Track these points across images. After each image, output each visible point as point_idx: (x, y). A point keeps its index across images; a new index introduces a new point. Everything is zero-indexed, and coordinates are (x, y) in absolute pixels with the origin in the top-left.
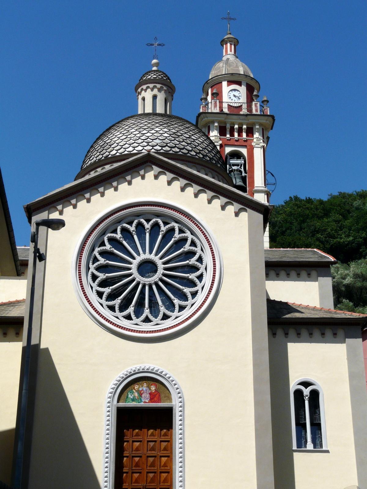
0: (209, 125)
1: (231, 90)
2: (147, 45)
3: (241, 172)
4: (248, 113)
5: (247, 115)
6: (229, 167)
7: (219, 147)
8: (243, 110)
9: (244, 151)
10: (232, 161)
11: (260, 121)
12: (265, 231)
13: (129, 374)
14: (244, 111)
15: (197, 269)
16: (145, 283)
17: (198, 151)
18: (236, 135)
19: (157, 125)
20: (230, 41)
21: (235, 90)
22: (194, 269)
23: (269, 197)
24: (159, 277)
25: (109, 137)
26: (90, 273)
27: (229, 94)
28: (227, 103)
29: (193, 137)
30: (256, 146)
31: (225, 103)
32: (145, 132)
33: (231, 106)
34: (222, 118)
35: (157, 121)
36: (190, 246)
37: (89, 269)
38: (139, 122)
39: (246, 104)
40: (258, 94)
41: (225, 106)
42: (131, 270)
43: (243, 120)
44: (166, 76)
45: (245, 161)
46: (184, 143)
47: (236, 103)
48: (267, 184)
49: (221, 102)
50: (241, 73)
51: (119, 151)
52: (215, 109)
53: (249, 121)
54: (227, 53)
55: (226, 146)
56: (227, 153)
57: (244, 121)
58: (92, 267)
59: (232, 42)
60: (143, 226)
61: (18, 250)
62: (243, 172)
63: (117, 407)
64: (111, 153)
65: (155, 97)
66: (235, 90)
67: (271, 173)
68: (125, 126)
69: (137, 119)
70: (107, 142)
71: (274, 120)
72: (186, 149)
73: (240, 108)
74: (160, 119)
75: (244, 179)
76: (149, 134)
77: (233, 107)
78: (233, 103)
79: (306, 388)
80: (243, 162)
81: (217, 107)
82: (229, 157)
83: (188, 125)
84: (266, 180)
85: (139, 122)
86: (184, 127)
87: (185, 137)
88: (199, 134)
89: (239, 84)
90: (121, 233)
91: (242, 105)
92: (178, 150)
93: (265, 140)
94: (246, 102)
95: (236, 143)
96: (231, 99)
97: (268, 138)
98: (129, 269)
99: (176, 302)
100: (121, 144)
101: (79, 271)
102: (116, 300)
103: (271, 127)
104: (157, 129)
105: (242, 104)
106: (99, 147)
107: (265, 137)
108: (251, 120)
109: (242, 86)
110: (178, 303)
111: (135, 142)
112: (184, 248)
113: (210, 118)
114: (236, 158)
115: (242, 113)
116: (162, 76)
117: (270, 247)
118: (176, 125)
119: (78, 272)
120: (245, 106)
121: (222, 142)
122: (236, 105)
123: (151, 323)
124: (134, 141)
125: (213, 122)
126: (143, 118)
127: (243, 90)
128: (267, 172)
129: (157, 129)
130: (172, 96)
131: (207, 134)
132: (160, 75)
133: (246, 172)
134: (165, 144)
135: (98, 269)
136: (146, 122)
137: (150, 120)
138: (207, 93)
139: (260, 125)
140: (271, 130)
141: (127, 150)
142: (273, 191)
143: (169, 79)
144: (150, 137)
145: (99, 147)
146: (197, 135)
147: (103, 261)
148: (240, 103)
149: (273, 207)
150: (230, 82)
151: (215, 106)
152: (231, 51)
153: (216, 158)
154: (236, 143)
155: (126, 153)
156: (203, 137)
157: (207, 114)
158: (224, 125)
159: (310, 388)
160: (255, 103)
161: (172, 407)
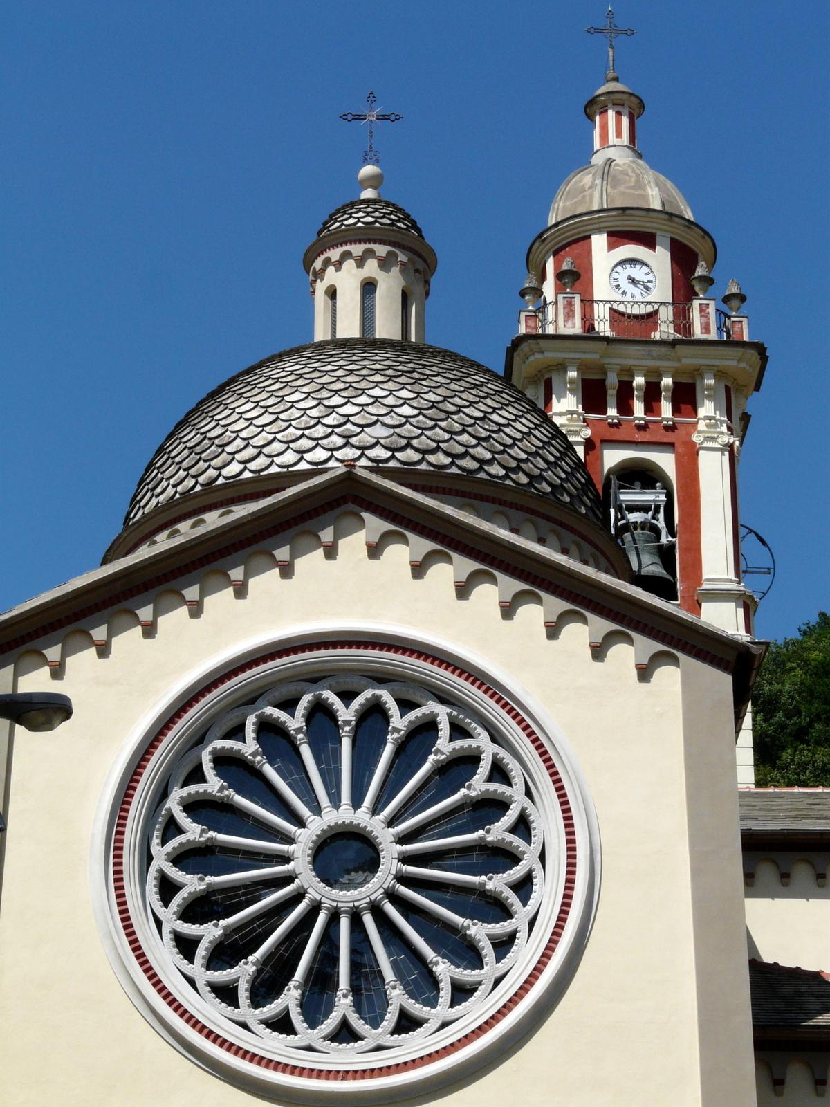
0: (546, 377)
4: (679, 336)
5: (673, 343)
8: (663, 327)
9: (666, 462)
12: (741, 729)
17: (513, 464)
18: (639, 408)
19: (378, 378)
21: (633, 262)
23: (751, 613)
27: (615, 275)
28: (608, 306)
29: (495, 417)
30: (706, 445)
31: (601, 305)
33: (622, 314)
34: (592, 353)
36: (490, 779)
38: (316, 369)
39: (671, 308)
41: (601, 313)
43: (660, 358)
44: (407, 217)
45: (670, 496)
46: (465, 438)
47: (636, 302)
49: (588, 302)
50: (652, 207)
51: (253, 466)
55: (605, 445)
60: (331, 714)
62: (664, 532)
64: (225, 472)
65: (369, 287)
66: (633, 262)
67: (756, 534)
71: (764, 359)
72: (474, 458)
73: (651, 320)
75: (666, 556)
76: (349, 410)
77: (629, 316)
78: (629, 305)
80: (663, 497)
82: (615, 482)
85: (316, 369)
88: (516, 405)
89: (648, 240)
91: (656, 312)
93: (737, 425)
96: (621, 291)
97: (746, 418)
98: (286, 859)
100: (258, 441)
102: (241, 964)
104: (377, 392)
105: (656, 307)
106: (186, 452)
107: (736, 415)
108: (690, 359)
111: (303, 435)
113: (552, 354)
115: (656, 336)
117: (759, 784)
118: (439, 379)
120: (666, 314)
122: (636, 310)
123: (360, 1042)
124: (299, 433)
125: (562, 367)
126: (332, 356)
127: (660, 260)
128: (742, 531)
129: (377, 392)
130: (427, 282)
133: (672, 533)
134: (403, 442)
135: (181, 859)
136: (341, 367)
137: (353, 362)
139: (720, 374)
141: (277, 460)
142: (765, 594)
143: (414, 226)
145: (186, 452)
148: (649, 303)
151: (569, 314)
152: (619, 134)
154: (639, 436)
157: (541, 341)
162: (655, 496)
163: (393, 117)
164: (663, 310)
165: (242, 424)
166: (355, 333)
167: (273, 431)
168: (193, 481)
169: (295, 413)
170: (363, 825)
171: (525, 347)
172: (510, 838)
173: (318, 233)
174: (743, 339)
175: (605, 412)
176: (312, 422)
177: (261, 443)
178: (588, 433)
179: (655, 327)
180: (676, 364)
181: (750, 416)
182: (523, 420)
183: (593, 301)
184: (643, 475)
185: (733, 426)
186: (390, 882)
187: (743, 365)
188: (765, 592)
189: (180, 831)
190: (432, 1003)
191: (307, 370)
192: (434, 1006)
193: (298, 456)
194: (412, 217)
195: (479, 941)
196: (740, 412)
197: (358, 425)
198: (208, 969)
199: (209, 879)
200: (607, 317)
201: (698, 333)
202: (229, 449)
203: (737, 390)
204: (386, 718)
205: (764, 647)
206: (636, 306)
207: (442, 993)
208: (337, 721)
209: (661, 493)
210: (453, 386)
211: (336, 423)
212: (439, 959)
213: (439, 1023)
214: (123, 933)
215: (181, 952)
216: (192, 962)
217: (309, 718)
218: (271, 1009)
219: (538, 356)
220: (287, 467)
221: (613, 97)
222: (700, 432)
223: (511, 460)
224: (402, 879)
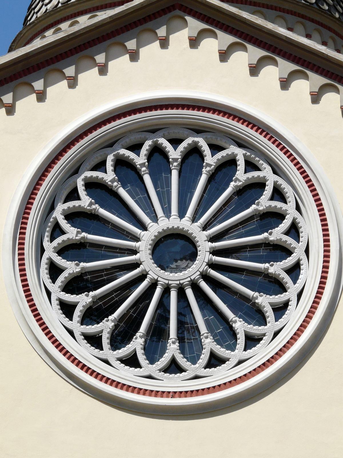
37: (43, 250)
212: (237, 319)
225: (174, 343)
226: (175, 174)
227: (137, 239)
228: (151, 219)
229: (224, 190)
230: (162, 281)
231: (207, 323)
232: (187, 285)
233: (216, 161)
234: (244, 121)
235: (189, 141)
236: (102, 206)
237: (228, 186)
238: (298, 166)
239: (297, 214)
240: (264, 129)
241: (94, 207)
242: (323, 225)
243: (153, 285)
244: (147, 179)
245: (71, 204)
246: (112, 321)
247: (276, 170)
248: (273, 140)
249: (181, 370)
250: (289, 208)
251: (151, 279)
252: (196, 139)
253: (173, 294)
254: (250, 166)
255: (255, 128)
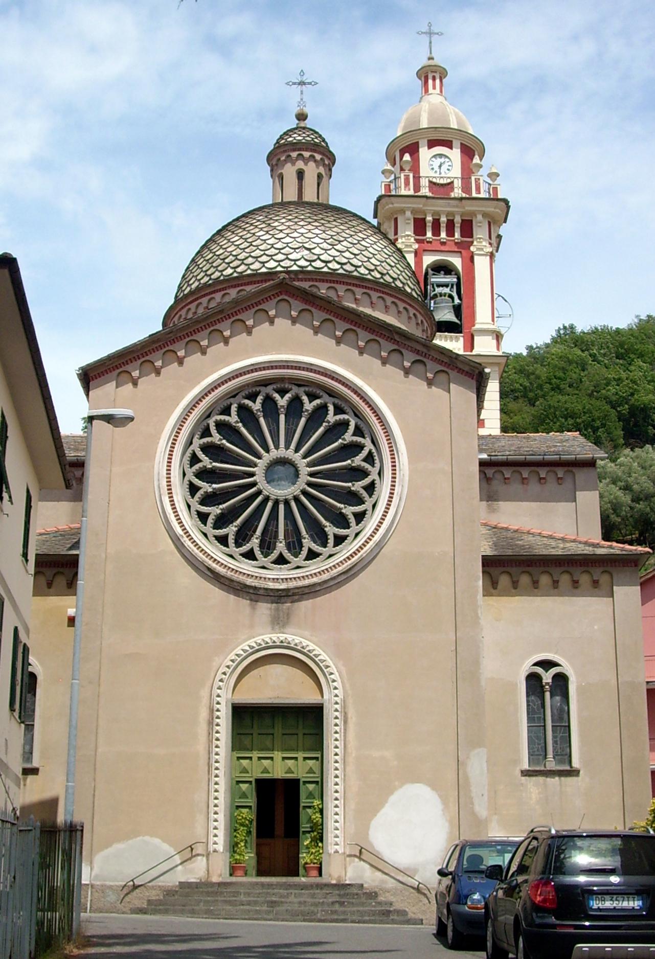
0: (395, 216)
1: (435, 156)
2: (287, 84)
3: (451, 296)
4: (464, 195)
5: (461, 199)
6: (430, 290)
7: (413, 255)
8: (456, 190)
9: (457, 262)
10: (435, 279)
11: (484, 209)
12: (482, 408)
13: (278, 644)
14: (457, 192)
15: (366, 474)
16: (277, 499)
17: (373, 268)
18: (443, 235)
19: (302, 223)
20: (432, 72)
21: (441, 156)
22: (360, 473)
23: (500, 341)
24: (295, 494)
25: (221, 244)
26: (190, 451)
27: (431, 163)
28: (427, 179)
29: (363, 243)
30: (477, 252)
31: (424, 178)
32: (281, 235)
33: (435, 184)
34: (418, 205)
35: (302, 217)
36: (354, 435)
37: (191, 443)
38: (271, 219)
39: (460, 180)
40: (482, 163)
41: (424, 182)
42: (255, 478)
43: (454, 206)
44: (320, 136)
45: (459, 278)
46: (347, 254)
47: (442, 177)
48: (498, 317)
49: (417, 178)
50: (452, 127)
51: (239, 270)
52: (407, 189)
53: (464, 208)
54: (428, 91)
55: (425, 253)
56: (428, 267)
57: (456, 209)
58: (197, 442)
59: (436, 72)
60: (274, 402)
61: (63, 441)
62: (456, 297)
63: (232, 704)
64: (224, 273)
65: (300, 174)
66: (441, 156)
67: (503, 298)
68: (248, 225)
69: (268, 212)
70: (217, 253)
71: (508, 207)
72: (352, 265)
73: (450, 186)
74: (309, 213)
75: (457, 310)
76: (288, 240)
77: (438, 184)
78: (438, 179)
79: (547, 671)
80: (455, 280)
81: (409, 184)
82: (430, 272)
83: (354, 223)
84: (495, 310)
85: (271, 219)
86: (349, 226)
87: (349, 242)
88: (374, 236)
89: (448, 144)
90: (238, 415)
91: (452, 182)
92: (338, 266)
93: (494, 240)
94: (460, 176)
95: (443, 248)
96: (434, 171)
97: (499, 237)
98: (252, 475)
99: (308, 543)
100: (241, 257)
101: (174, 442)
102: (230, 526)
103: (503, 219)
104: (302, 231)
105: (452, 180)
106: (205, 263)
107: (493, 237)
108: (469, 207)
109: (454, 149)
110: (308, 545)
111: (264, 254)
112: (344, 439)
113: (398, 204)
114: (442, 272)
115: (452, 195)
116: (312, 136)
117: (504, 429)
118: (334, 223)
119: (171, 441)
120: (458, 184)
121: (419, 247)
122: (442, 181)
123: (288, 565)
124: (262, 253)
125: (403, 211)
126: (279, 211)
127: (455, 154)
128: (495, 296)
129: (302, 231)
130: (330, 170)
131: (392, 236)
132: (308, 136)
133: (460, 298)
134: (316, 257)
135: (205, 449)
136: (284, 218)
137: (290, 215)
138: (393, 160)
139: (485, 215)
140: (504, 224)
141: (251, 267)
142: (509, 328)
143: (324, 140)
144: (289, 245)
145: (205, 263)
146: (371, 238)
147: (218, 439)
148: (449, 178)
149: (506, 358)
150: (432, 144)
151: (407, 183)
152: (434, 88)
153: (403, 277)
154: (443, 248)
155: (249, 272)
156: (381, 241)
157: (391, 198)
158: (424, 217)
159: (554, 671)
160: (475, 179)
161: (323, 704)
162: (452, 279)
163: (313, 83)
164: (456, 181)
165: (233, 248)
166: (295, 198)
167: (249, 251)
168: (208, 278)
169: (259, 242)
170: (290, 458)
171: (383, 201)
172: (364, 464)
173: (269, 158)
174: (497, 196)
175: (425, 234)
176: (269, 247)
177: (243, 258)
178: (416, 246)
179: (452, 189)
180: (461, 210)
181: (502, 236)
182: (378, 244)
183: (420, 177)
184: (443, 268)
185: (492, 242)
186: (298, 492)
187: (497, 210)
188: (509, 326)
189: (199, 461)
190: (296, 555)
191: (266, 219)
192: (296, 557)
193: (262, 265)
194: (323, 136)
195: (347, 515)
196: (496, 235)
197: (292, 248)
198: (214, 529)
199: (224, 441)
200: (427, 185)
201: (474, 195)
202: (227, 261)
203: (494, 223)
204: (302, 404)
205: (506, 358)
206: (442, 179)
207: (302, 552)
208: (277, 406)
209: (454, 278)
210: (342, 227)
211: (281, 247)
212: (307, 536)
213: (295, 566)
214: (166, 463)
215: (201, 520)
216: (205, 525)
217: (263, 404)
218: (245, 548)
219: (391, 206)
220: (256, 270)
221: (431, 68)
222: (474, 246)
223: (372, 266)
224: (310, 484)
225: (257, 538)
226: (303, 421)
227: (259, 457)
228: (275, 446)
229: (334, 443)
230: (265, 493)
231: (286, 532)
232: (282, 501)
233: (312, 407)
234: (379, 418)
235: (346, 417)
236: (244, 426)
237: (336, 441)
238: (392, 453)
239: (376, 477)
240: (385, 424)
241: (238, 425)
242: (391, 489)
243: (259, 493)
244: (282, 418)
245: (223, 417)
246: (221, 509)
247: (374, 442)
248: (389, 441)
249: (255, 559)
250: (374, 472)
251: (258, 488)
252: (351, 419)
253: (270, 504)
254: (358, 432)
255: (379, 421)
